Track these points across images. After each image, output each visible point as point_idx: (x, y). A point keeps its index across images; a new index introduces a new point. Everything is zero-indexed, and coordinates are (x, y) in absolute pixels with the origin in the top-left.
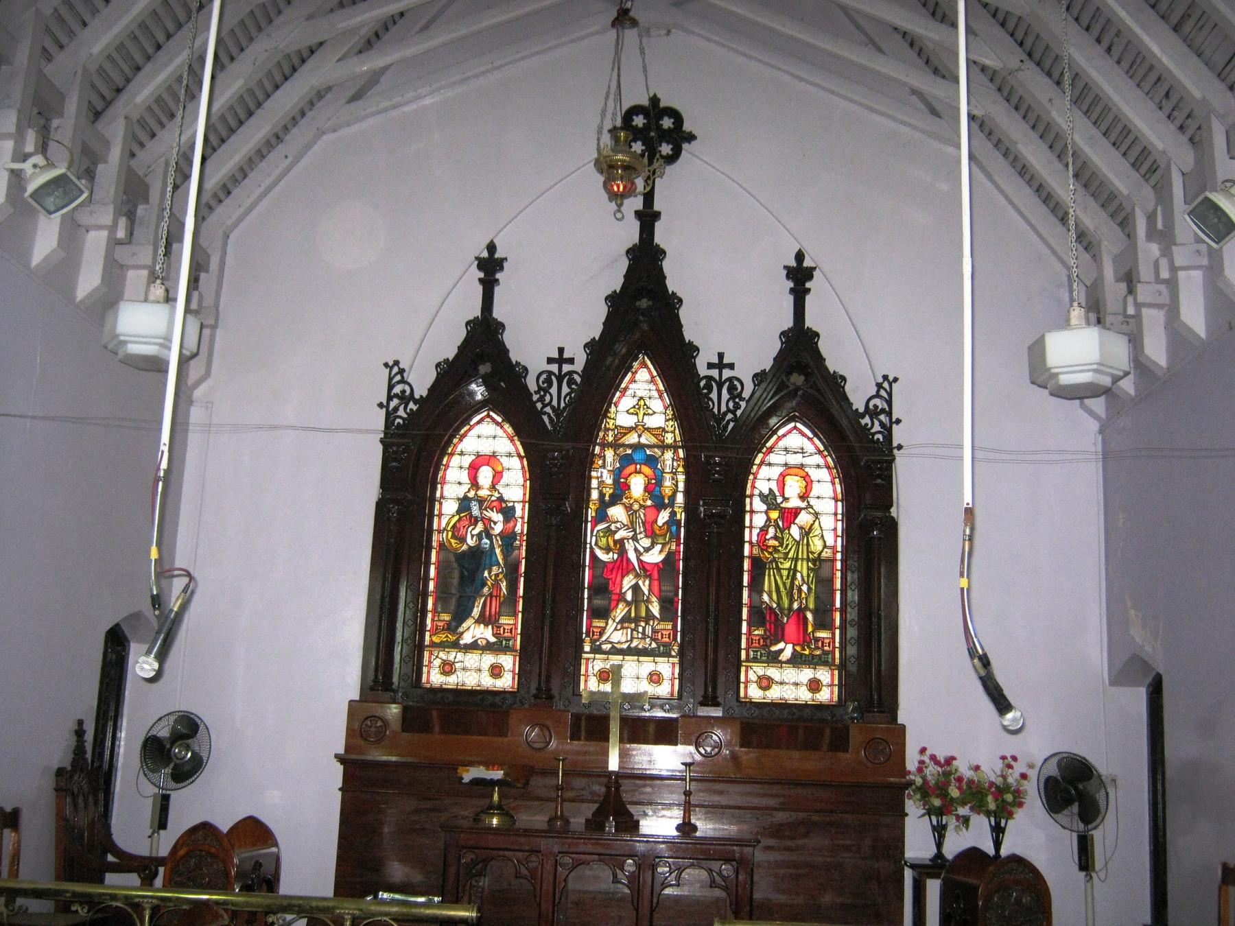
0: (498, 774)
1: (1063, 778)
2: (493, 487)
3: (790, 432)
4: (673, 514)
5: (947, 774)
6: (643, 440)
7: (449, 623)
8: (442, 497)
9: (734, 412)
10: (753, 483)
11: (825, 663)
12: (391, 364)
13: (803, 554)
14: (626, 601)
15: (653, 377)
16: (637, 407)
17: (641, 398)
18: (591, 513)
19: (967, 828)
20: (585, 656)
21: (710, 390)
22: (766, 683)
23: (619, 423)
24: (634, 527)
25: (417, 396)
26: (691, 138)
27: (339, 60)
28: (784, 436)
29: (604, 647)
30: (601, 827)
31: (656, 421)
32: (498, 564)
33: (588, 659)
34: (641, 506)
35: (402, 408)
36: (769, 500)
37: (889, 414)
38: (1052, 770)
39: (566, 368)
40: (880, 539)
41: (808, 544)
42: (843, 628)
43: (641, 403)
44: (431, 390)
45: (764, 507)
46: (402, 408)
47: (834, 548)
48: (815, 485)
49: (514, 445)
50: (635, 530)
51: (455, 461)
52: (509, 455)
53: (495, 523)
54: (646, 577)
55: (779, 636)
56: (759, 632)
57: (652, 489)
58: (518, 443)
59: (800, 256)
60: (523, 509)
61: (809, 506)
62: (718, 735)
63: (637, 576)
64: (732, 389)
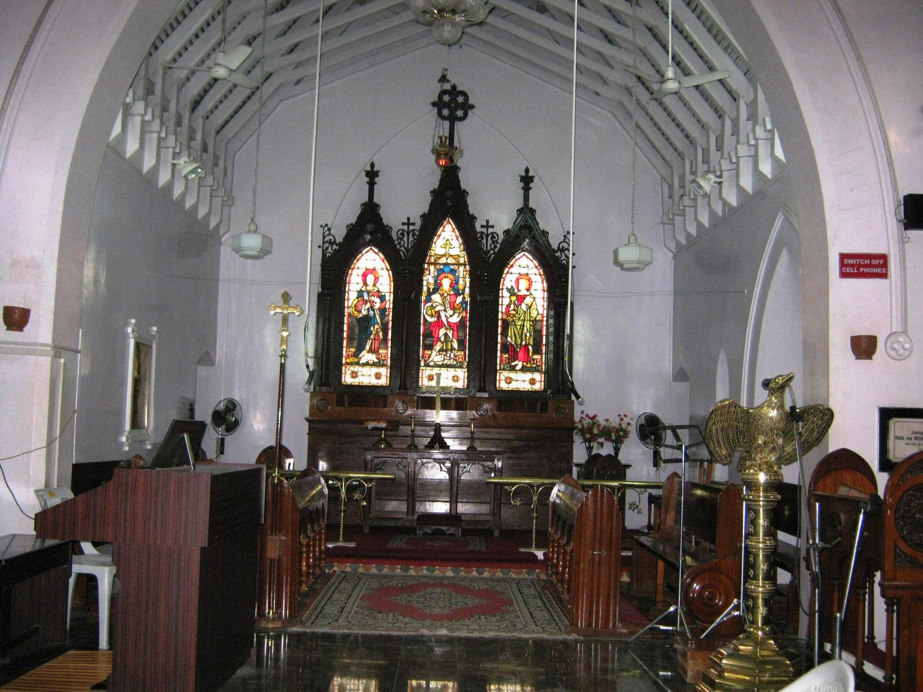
0: (384, 425)
2: (374, 285)
4: (464, 298)
7: (354, 353)
11: (538, 371)
13: (527, 317)
18: (423, 298)
22: (509, 381)
24: (444, 303)
25: (337, 242)
26: (472, 107)
36: (511, 291)
39: (411, 228)
42: (546, 353)
43: (448, 242)
44: (345, 239)
51: (355, 272)
55: (514, 357)
56: (507, 356)
57: (454, 285)
59: (527, 170)
62: (486, 406)
63: (447, 329)
64: (493, 237)
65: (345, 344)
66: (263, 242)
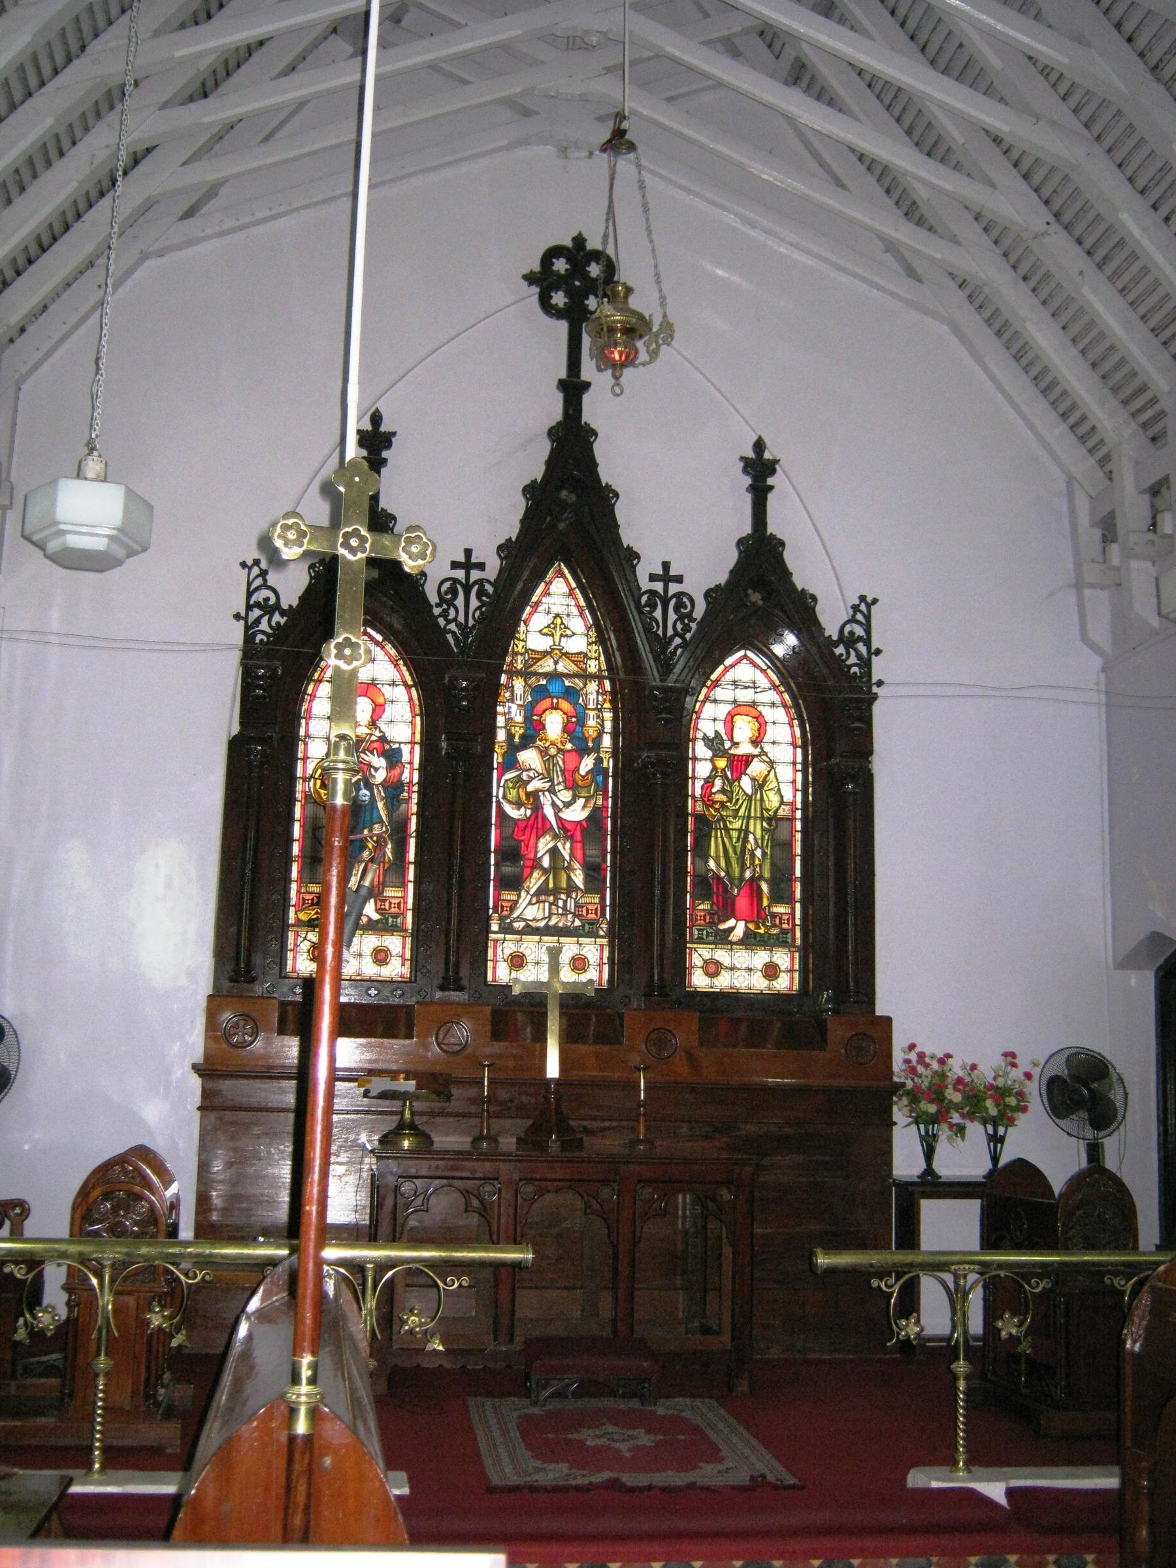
1: (1072, 1077)
2: (373, 723)
3: (739, 661)
4: (599, 760)
5: (943, 1076)
6: (561, 668)
8: (307, 736)
9: (682, 637)
10: (696, 723)
12: (250, 563)
14: (542, 868)
15: (571, 589)
16: (552, 626)
17: (557, 616)
18: (497, 759)
19: (963, 1137)
20: (492, 936)
21: (654, 607)
22: (713, 968)
23: (530, 645)
24: (550, 774)
25: (285, 606)
26: (530, 279)
27: (184, 164)
28: (732, 666)
29: (516, 925)
30: (542, 1146)
31: (577, 644)
32: (381, 821)
33: (496, 941)
34: (559, 750)
35: (265, 620)
36: (714, 743)
37: (868, 642)
38: (1059, 1068)
39: (475, 575)
40: (855, 794)
41: (762, 800)
43: (557, 621)
45: (709, 754)
46: (265, 620)
47: (792, 804)
48: (769, 728)
49: (399, 671)
50: (551, 780)
52: (393, 684)
53: (376, 769)
54: (566, 838)
55: (727, 909)
56: (705, 906)
58: (404, 669)
59: (759, 446)
60: (412, 752)
61: (763, 753)
63: (556, 837)
65: (294, 874)
66: (127, 510)
